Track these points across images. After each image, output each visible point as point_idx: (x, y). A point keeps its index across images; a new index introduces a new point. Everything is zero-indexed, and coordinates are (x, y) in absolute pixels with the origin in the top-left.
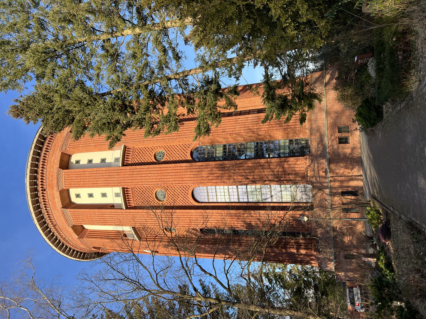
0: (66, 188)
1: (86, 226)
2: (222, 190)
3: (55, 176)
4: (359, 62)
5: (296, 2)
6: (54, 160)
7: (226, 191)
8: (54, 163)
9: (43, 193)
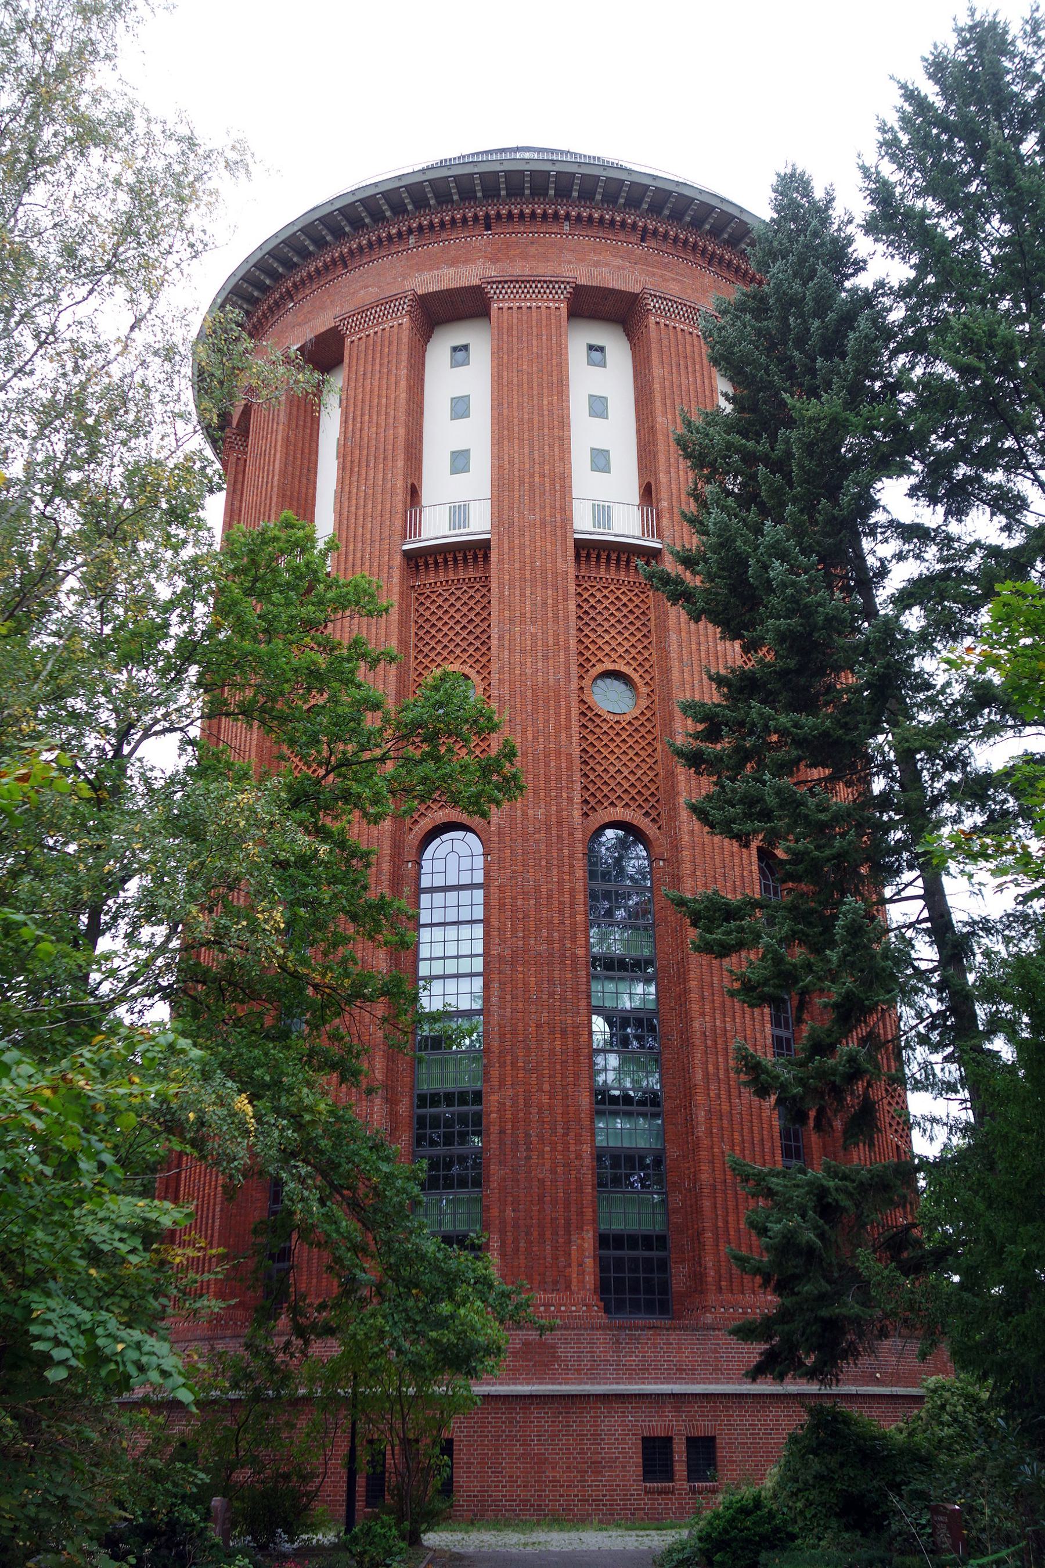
0: (494, 312)
1: (337, 381)
2: (465, 950)
3: (545, 270)
4: (941, 1519)
5: (8, 1317)
6: (607, 265)
7: (465, 966)
8: (596, 264)
9: (476, 218)
